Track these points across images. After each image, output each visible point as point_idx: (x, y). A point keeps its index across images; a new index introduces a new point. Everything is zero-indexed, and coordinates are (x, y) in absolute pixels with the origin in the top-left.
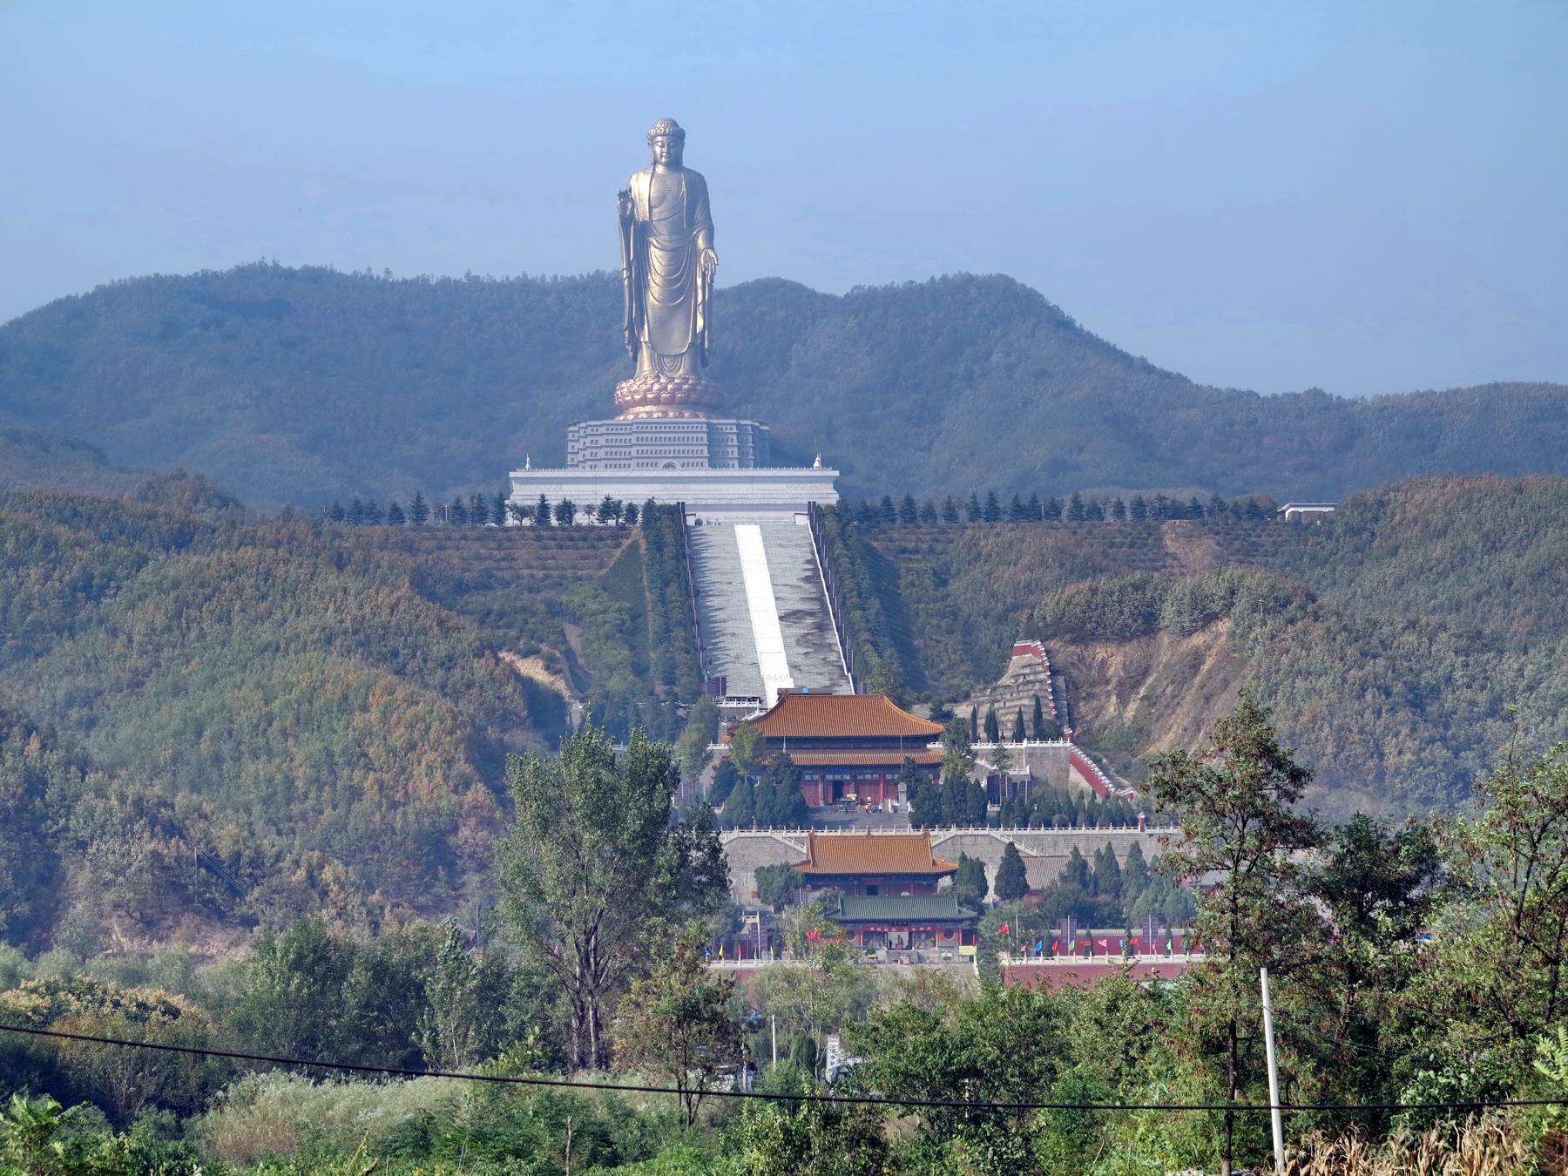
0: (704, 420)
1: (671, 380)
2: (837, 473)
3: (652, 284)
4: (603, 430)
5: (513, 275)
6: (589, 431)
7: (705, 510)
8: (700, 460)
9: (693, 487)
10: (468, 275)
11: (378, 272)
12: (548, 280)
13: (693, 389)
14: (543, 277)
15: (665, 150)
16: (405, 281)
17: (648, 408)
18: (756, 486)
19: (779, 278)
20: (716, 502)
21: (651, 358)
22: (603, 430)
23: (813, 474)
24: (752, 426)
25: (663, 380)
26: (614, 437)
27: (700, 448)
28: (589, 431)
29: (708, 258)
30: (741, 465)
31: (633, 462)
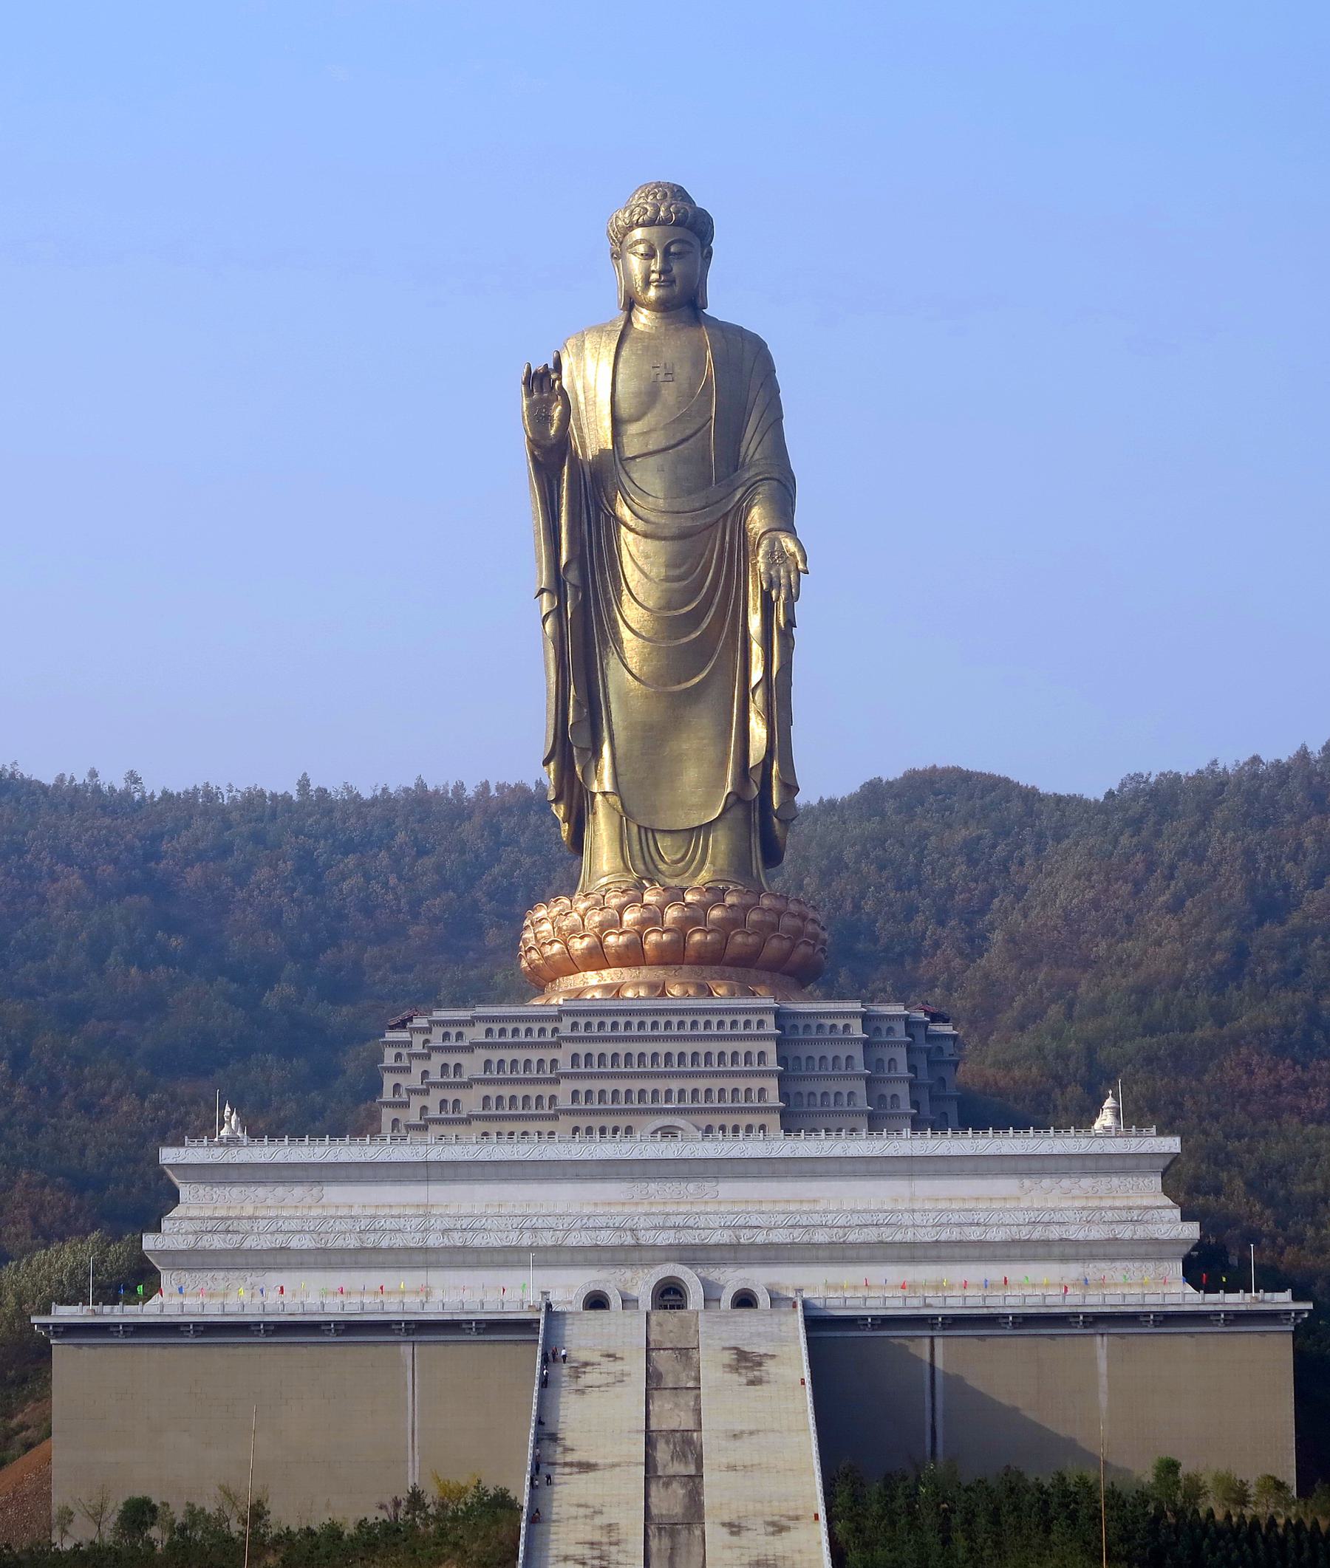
0: (769, 1002)
1: (676, 895)
2: (1172, 1144)
3: (626, 634)
4: (476, 1034)
5: (398, 780)
6: (436, 1039)
7: (765, 1261)
8: (756, 1120)
9: (728, 1189)
10: (304, 784)
11: (113, 779)
12: (470, 792)
13: (734, 922)
14: (460, 787)
15: (656, 265)
16: (167, 796)
17: (609, 976)
18: (925, 1187)
19: (957, 770)
20: (798, 1236)
21: (622, 839)
22: (476, 1034)
23: (1096, 1147)
24: (909, 1023)
25: (649, 897)
26: (508, 1055)
27: (755, 1084)
28: (436, 1038)
29: (777, 556)
30: (875, 1123)
31: (566, 1123)
